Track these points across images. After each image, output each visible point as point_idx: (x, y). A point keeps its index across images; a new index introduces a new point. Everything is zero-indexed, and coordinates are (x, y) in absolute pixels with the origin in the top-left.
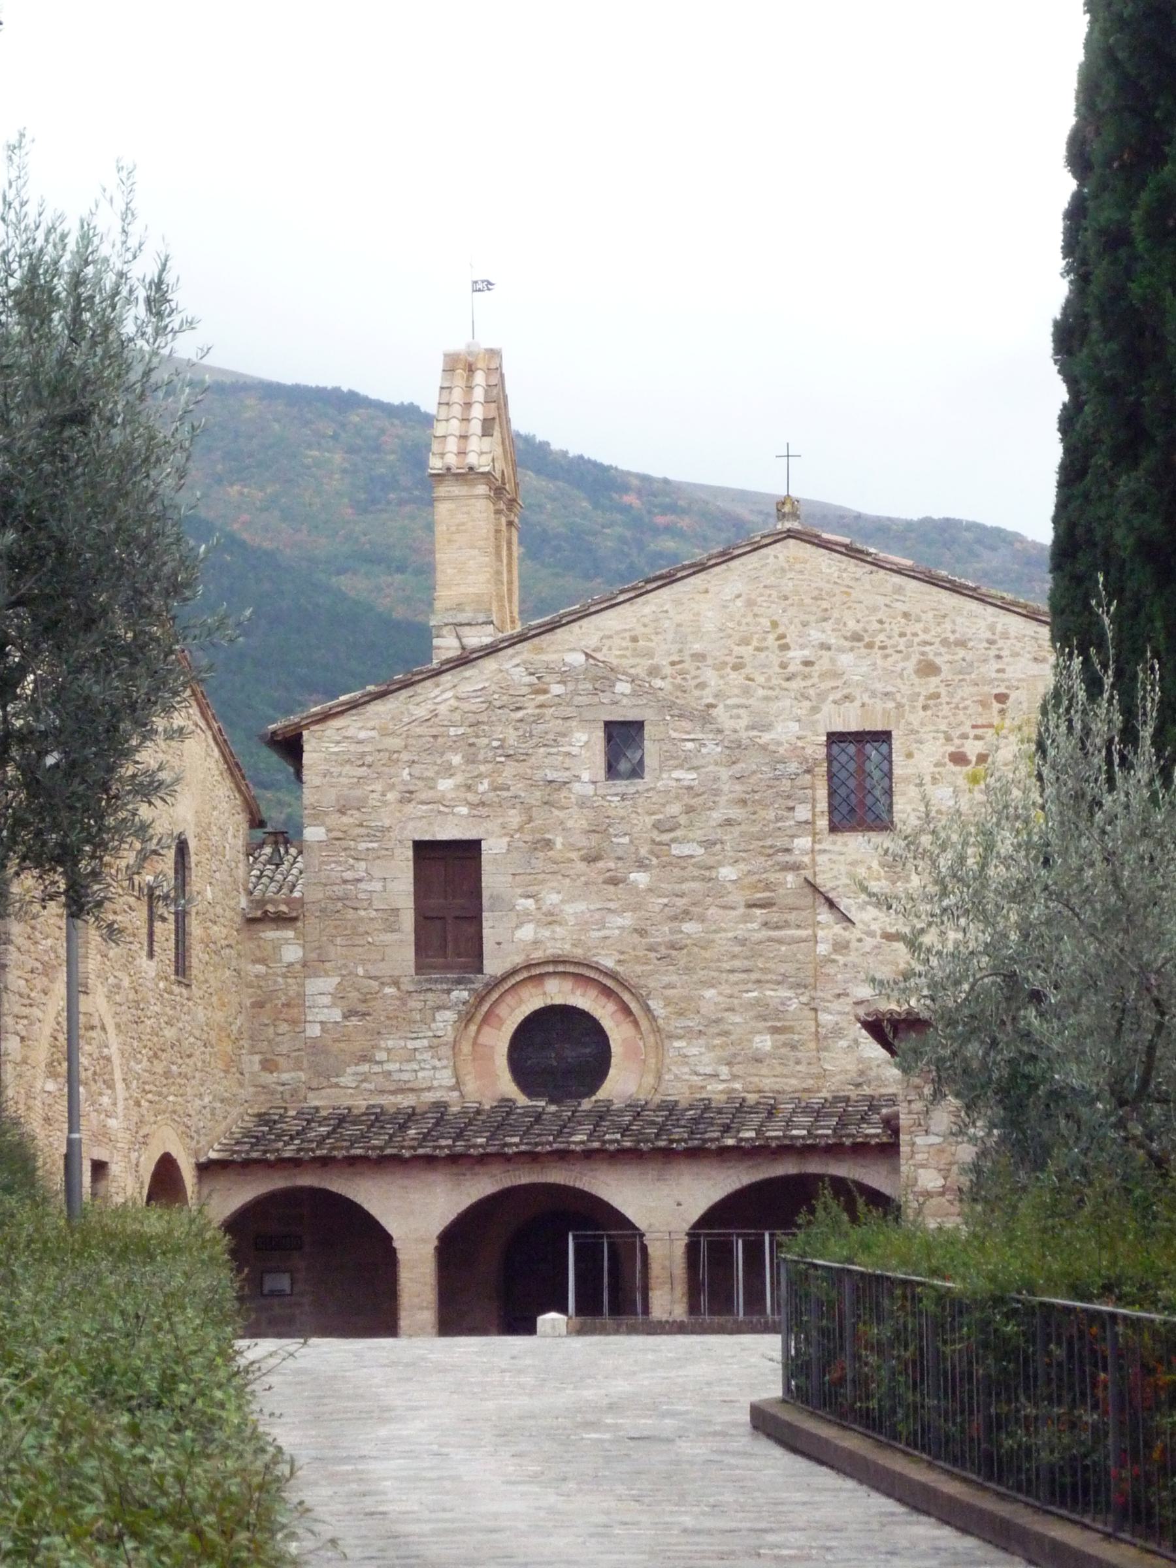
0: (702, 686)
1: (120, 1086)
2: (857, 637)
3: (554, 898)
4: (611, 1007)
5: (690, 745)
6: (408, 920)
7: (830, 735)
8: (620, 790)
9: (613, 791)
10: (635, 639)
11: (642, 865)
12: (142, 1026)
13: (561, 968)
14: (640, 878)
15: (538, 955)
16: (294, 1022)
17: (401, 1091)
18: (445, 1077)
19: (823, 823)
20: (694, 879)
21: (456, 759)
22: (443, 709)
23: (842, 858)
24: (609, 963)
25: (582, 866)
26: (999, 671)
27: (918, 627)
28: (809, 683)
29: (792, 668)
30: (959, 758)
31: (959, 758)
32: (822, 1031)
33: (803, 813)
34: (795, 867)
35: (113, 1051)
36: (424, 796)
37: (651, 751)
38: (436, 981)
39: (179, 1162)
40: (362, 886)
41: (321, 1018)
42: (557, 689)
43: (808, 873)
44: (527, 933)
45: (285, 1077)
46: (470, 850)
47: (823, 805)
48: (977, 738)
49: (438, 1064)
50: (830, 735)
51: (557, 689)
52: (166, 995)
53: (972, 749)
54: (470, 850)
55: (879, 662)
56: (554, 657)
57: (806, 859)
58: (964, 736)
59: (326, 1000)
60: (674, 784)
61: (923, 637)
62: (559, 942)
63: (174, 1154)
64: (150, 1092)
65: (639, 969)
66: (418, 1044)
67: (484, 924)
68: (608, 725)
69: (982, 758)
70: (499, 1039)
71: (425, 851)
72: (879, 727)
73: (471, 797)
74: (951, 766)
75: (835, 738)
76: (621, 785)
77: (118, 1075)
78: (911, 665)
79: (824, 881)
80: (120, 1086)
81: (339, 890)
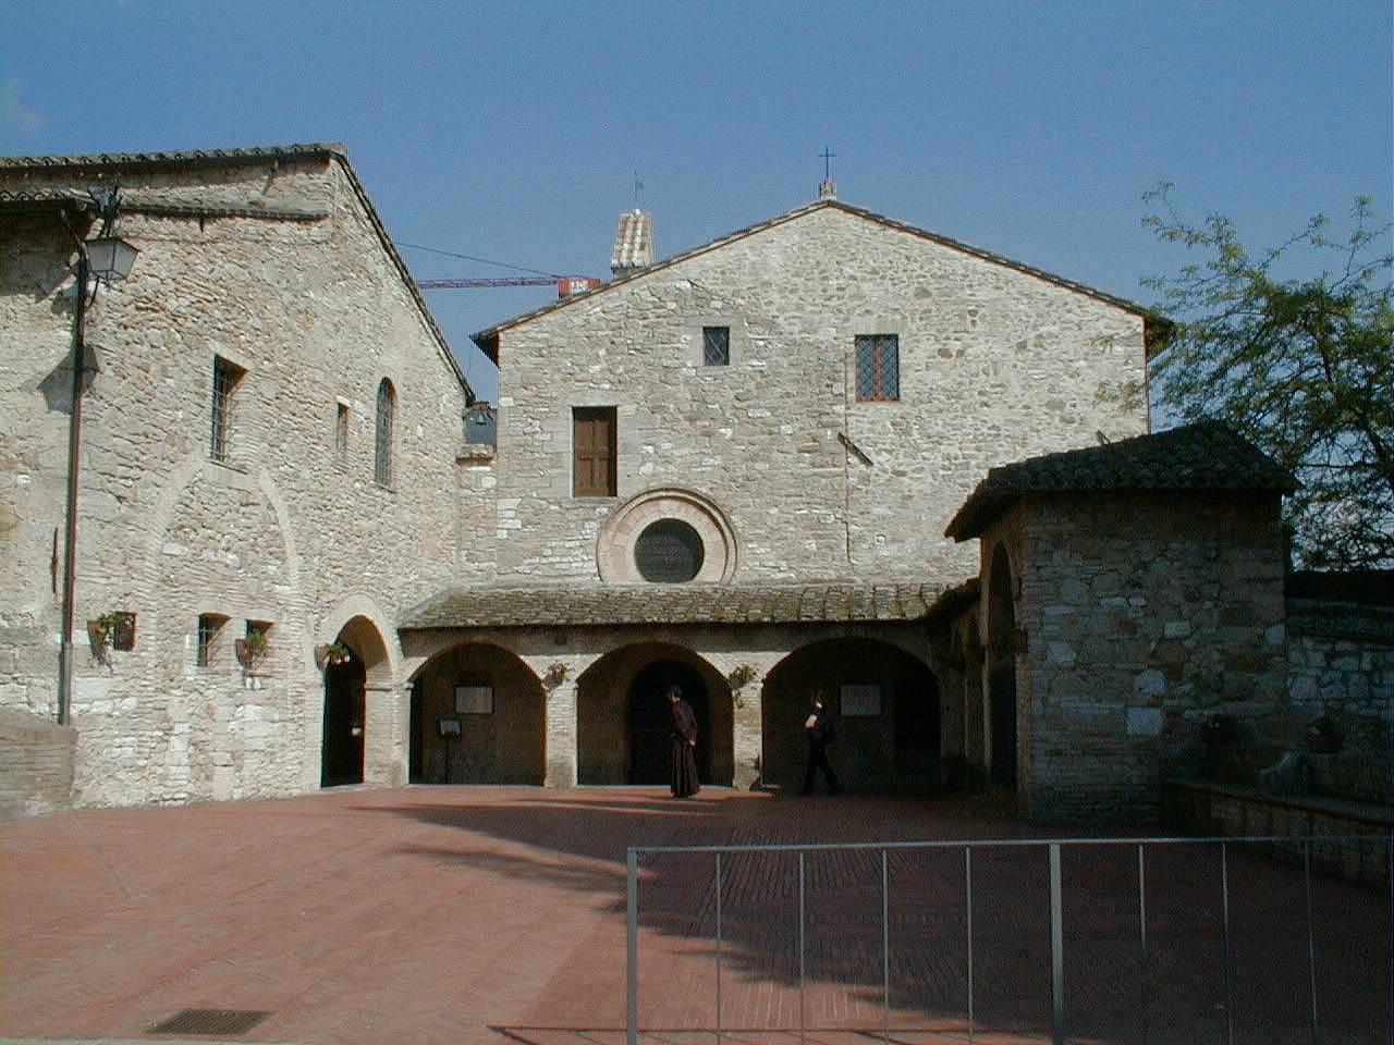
0: (770, 303)
1: (294, 561)
2: (874, 272)
3: (667, 445)
4: (706, 519)
5: (761, 343)
6: (569, 460)
7: (857, 337)
8: (713, 373)
9: (709, 373)
10: (723, 273)
11: (727, 424)
12: (326, 514)
13: (671, 494)
14: (729, 432)
15: (654, 484)
16: (488, 529)
17: (559, 576)
18: (591, 567)
19: (852, 395)
20: (763, 433)
21: (602, 352)
22: (592, 319)
23: (865, 419)
24: (704, 490)
25: (687, 424)
26: (970, 295)
27: (915, 266)
28: (841, 302)
29: (829, 293)
30: (944, 353)
31: (944, 353)
32: (851, 537)
33: (839, 388)
34: (833, 425)
35: (285, 525)
36: (579, 377)
37: (734, 348)
38: (584, 502)
39: (376, 623)
40: (537, 436)
41: (506, 526)
42: (673, 305)
43: (840, 429)
44: (648, 468)
45: (483, 565)
46: (608, 415)
47: (852, 384)
48: (956, 339)
49: (586, 558)
50: (857, 337)
51: (673, 305)
52: (362, 494)
53: (954, 346)
54: (608, 415)
55: (891, 288)
56: (668, 284)
57: (842, 420)
58: (948, 338)
59: (511, 514)
60: (750, 368)
61: (919, 272)
62: (671, 476)
63: (370, 617)
64: (340, 567)
65: (724, 494)
66: (572, 544)
67: (619, 462)
68: (704, 328)
69: (961, 353)
70: (629, 542)
71: (581, 414)
72: (890, 332)
73: (611, 377)
74: (940, 359)
75: (860, 338)
76: (717, 370)
77: (290, 548)
78: (911, 291)
79: (853, 436)
80: (294, 561)
81: (521, 440)
